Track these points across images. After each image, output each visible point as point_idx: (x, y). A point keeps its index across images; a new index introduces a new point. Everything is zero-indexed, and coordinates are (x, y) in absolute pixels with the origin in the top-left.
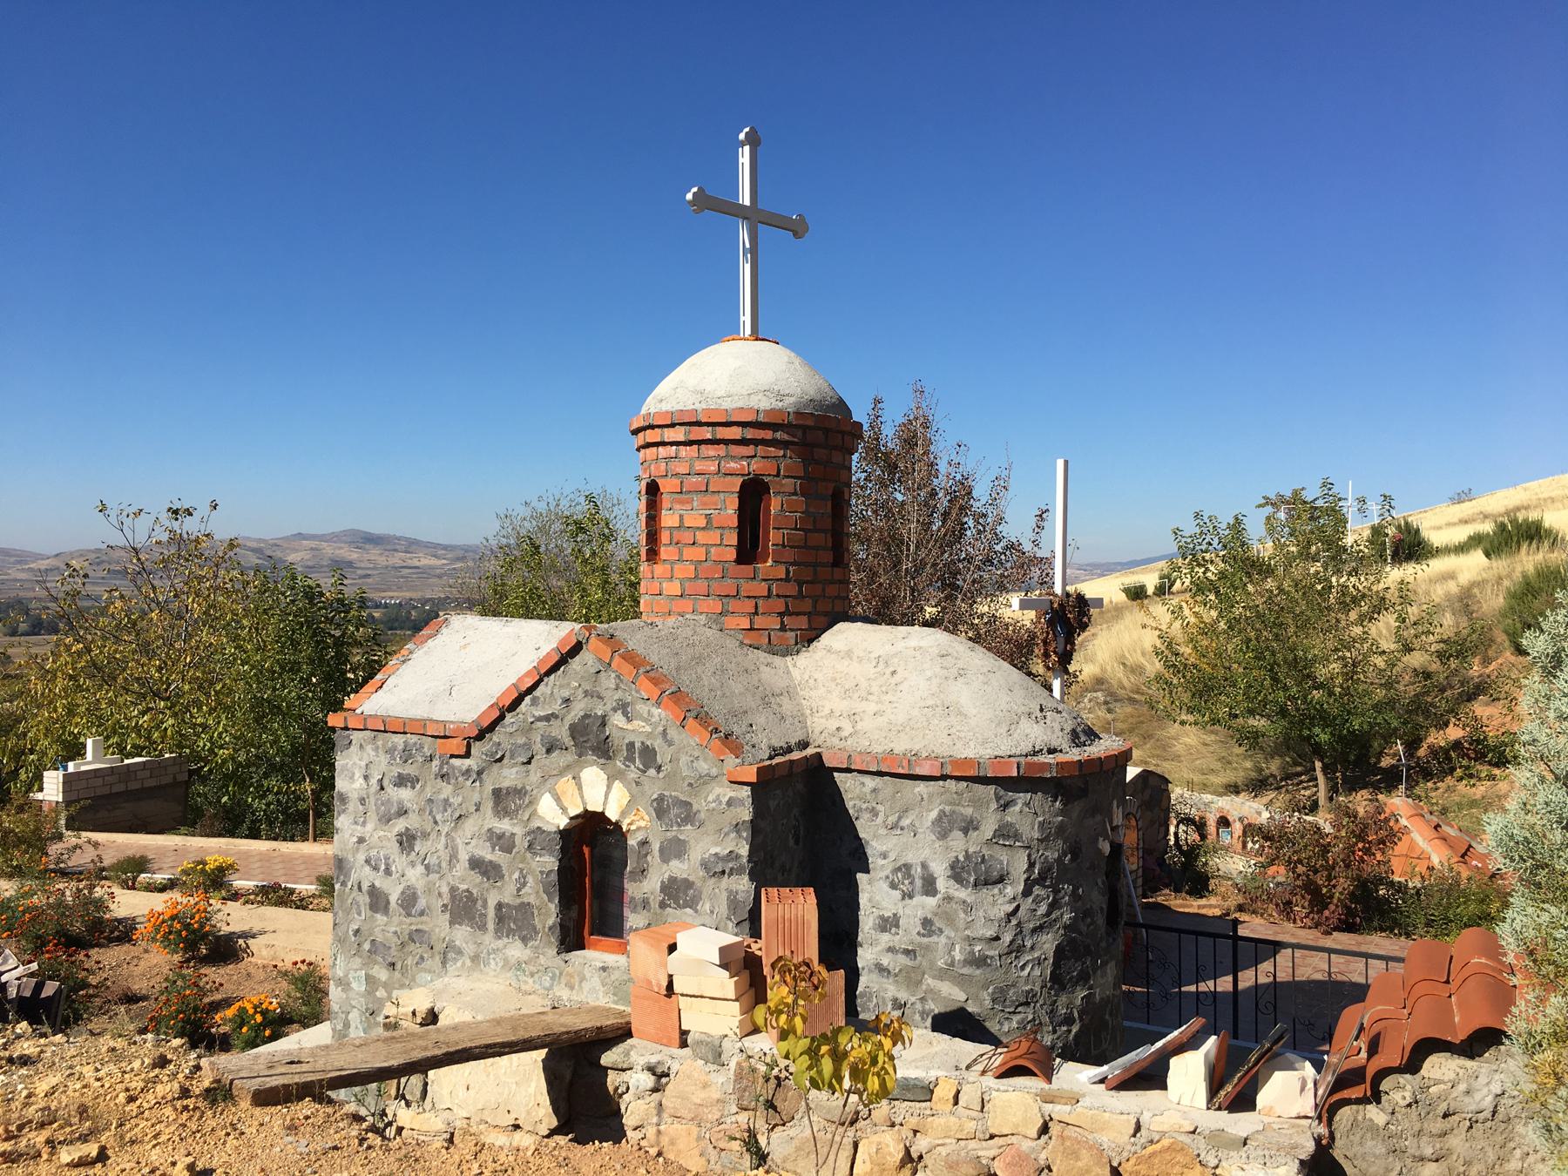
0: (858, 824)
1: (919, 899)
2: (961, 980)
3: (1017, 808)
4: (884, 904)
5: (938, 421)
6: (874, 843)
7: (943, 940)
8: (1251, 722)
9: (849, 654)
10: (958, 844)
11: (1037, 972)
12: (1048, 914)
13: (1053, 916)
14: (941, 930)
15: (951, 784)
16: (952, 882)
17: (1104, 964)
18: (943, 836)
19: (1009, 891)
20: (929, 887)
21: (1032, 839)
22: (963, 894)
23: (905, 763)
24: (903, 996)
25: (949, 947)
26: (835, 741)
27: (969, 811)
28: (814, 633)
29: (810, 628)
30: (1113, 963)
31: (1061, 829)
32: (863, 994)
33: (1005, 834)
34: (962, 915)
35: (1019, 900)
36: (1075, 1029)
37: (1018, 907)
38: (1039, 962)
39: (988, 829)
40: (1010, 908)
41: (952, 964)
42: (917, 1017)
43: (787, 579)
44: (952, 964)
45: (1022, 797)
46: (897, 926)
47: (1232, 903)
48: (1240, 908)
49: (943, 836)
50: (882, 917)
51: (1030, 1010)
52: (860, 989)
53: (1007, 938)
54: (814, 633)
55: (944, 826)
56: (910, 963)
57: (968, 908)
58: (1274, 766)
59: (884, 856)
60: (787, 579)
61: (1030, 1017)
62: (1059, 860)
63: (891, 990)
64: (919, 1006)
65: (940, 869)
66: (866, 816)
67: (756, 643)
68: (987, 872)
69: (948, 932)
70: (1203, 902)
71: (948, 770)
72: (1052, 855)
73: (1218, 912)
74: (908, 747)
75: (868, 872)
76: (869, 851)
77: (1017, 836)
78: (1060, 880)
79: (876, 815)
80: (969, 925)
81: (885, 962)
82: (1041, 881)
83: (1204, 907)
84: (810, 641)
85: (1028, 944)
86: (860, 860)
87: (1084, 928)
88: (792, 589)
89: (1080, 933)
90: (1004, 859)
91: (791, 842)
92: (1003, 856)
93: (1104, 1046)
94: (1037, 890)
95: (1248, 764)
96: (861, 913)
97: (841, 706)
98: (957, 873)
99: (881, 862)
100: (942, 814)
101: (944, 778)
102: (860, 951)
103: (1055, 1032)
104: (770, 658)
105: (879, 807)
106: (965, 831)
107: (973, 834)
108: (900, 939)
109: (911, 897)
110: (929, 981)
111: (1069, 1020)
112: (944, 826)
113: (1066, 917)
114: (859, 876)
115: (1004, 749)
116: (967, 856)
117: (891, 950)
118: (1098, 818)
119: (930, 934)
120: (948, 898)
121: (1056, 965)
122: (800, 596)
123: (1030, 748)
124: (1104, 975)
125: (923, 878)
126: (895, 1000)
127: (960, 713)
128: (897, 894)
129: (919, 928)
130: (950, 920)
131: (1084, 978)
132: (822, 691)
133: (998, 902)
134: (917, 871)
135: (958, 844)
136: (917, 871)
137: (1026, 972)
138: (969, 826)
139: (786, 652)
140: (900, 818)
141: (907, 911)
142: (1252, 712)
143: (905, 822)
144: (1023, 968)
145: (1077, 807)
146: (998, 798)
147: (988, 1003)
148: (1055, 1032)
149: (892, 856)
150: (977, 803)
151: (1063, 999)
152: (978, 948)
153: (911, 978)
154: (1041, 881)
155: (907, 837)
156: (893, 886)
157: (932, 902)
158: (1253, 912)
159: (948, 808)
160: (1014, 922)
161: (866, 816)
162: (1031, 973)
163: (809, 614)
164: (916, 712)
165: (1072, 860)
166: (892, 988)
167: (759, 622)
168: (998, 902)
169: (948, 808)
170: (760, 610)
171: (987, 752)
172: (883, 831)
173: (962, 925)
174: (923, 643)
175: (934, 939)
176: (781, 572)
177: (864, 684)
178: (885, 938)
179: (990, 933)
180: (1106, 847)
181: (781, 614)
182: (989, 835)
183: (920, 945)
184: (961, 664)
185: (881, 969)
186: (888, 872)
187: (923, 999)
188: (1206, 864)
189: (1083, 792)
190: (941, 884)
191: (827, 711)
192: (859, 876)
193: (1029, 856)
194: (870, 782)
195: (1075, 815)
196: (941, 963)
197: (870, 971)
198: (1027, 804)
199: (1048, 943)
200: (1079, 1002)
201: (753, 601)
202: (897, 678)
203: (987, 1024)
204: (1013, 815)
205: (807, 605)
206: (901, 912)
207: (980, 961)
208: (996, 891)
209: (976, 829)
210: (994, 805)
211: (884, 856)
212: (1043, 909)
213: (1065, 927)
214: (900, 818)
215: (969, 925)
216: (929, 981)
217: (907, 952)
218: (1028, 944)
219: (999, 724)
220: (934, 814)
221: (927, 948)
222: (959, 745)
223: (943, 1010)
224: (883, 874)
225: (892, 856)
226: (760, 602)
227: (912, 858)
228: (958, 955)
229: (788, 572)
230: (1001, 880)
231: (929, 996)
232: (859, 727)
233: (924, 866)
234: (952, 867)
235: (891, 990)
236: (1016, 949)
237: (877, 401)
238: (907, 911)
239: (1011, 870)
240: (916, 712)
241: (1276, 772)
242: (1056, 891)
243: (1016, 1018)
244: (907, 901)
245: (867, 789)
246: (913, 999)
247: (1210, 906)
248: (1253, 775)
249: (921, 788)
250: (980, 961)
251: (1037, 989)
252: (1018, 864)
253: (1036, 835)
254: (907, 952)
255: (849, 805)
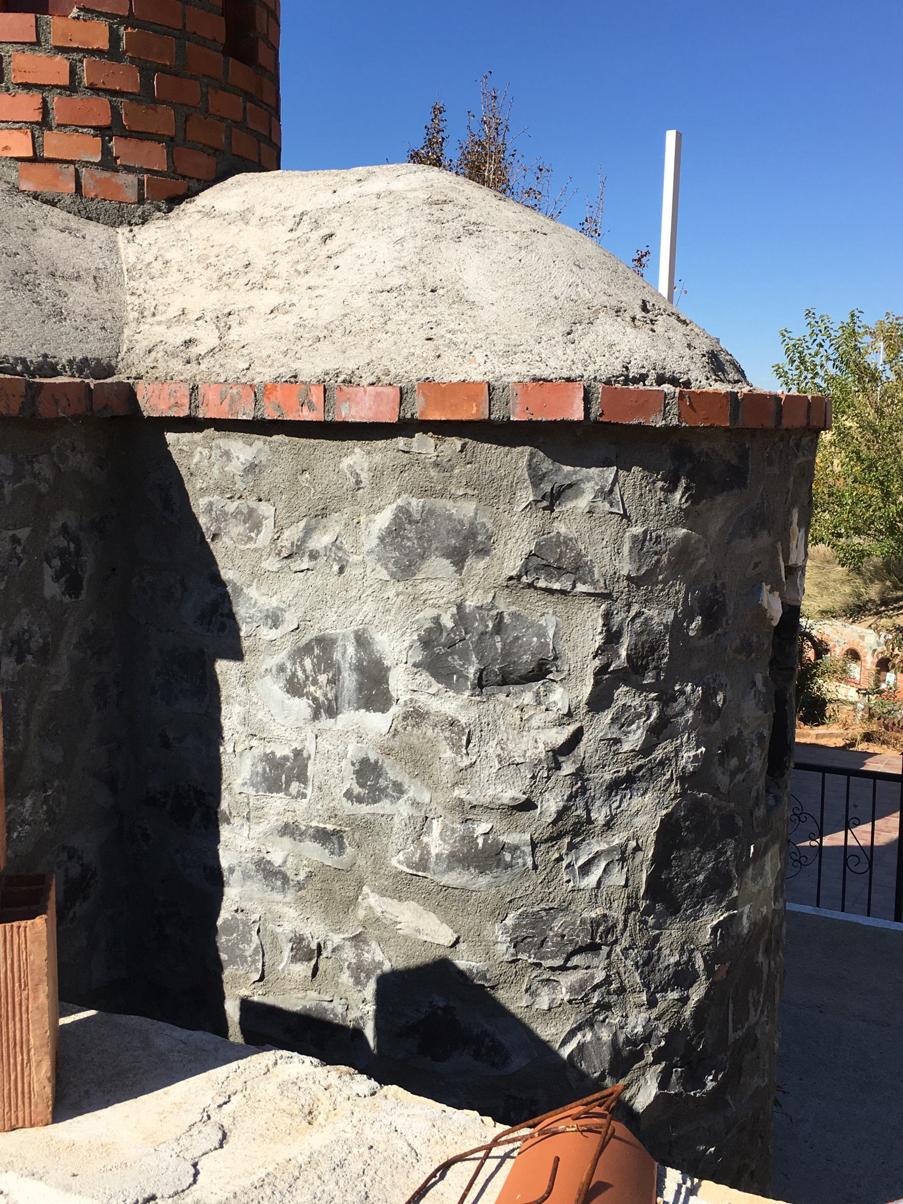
0: (218, 549)
1: (352, 717)
2: (442, 900)
3: (582, 503)
4: (276, 730)
5: (512, 141)
6: (252, 592)
7: (403, 808)
8: (856, 540)
9: (244, 216)
10: (441, 589)
11: (617, 878)
12: (646, 749)
13: (658, 754)
14: (399, 789)
15: (424, 445)
16: (424, 677)
17: (760, 854)
18: (406, 569)
19: (559, 698)
20: (374, 690)
21: (615, 577)
22: (451, 704)
23: (316, 396)
24: (315, 930)
25: (418, 824)
26: (176, 365)
27: (466, 510)
28: (181, 186)
29: (173, 172)
30: (776, 848)
31: (683, 555)
32: (231, 927)
33: (551, 565)
34: (448, 754)
35: (582, 718)
36: (696, 994)
37: (577, 736)
38: (623, 855)
39: (511, 556)
40: (560, 736)
41: (423, 864)
42: (346, 978)
43: (113, 53)
44: (423, 864)
45: (594, 478)
46: (302, 777)
47: (858, 730)
48: (868, 737)
49: (406, 569)
50: (269, 759)
51: (599, 961)
52: (225, 914)
53: (551, 804)
54: (181, 186)
55: (408, 547)
56: (331, 861)
57: (463, 736)
58: (873, 592)
59: (274, 619)
60: (113, 53)
61: (600, 976)
62: (676, 629)
63: (291, 918)
64: (349, 954)
65: (396, 647)
66: (236, 529)
67: (47, 191)
68: (506, 654)
69: (415, 790)
70: (821, 730)
71: (420, 408)
72: (660, 616)
73: (840, 743)
74: (331, 366)
75: (237, 654)
76: (241, 611)
77: (579, 569)
78: (676, 672)
79: (257, 526)
80: (463, 775)
81: (276, 858)
82: (632, 674)
83: (824, 736)
84: (174, 200)
85: (599, 816)
86: (217, 627)
87: (723, 780)
88: (125, 78)
89: (715, 790)
90: (549, 623)
91: (52, 589)
92: (546, 617)
93: (753, 1018)
94: (623, 696)
95: (847, 589)
96: (226, 749)
97: (200, 298)
98: (437, 655)
99: (268, 634)
100: (403, 518)
101: (406, 427)
102: (225, 832)
103: (652, 1003)
104: (75, 222)
105: (266, 509)
106: (458, 557)
107: (476, 565)
108: (306, 809)
109: (332, 712)
110: (373, 901)
111: (683, 977)
112: (408, 547)
113: (687, 755)
114: (223, 667)
115: (557, 362)
116: (462, 616)
117: (288, 830)
118: (764, 539)
119: (375, 795)
120: (416, 715)
121: (661, 860)
122: (144, 96)
123: (618, 369)
124: (760, 873)
125: (359, 669)
126: (298, 941)
127: (460, 299)
128: (301, 706)
129: (350, 783)
130: (420, 764)
131: (718, 886)
132: (174, 278)
133: (531, 725)
134: (347, 654)
135: (441, 589)
136: (347, 654)
137: (591, 880)
138: (466, 547)
139: (119, 217)
140: (308, 532)
141: (325, 745)
142: (858, 531)
143: (321, 541)
144: (585, 869)
145: (720, 511)
146: (537, 478)
147: (503, 949)
148: (652, 1003)
149: (291, 620)
150: (487, 490)
151: (673, 933)
152: (482, 828)
153: (333, 892)
154: (632, 674)
155: (325, 577)
156: (294, 688)
157: (377, 723)
158: (883, 743)
159: (416, 504)
160: (568, 768)
161: (236, 529)
162: (601, 881)
163: (170, 142)
164: (361, 301)
165: (705, 629)
166: (291, 913)
167: (55, 144)
168: (531, 725)
169: (416, 504)
170: (56, 118)
171: (514, 371)
172: (271, 564)
173: (445, 773)
174: (398, 185)
175: (384, 806)
176: (97, 35)
177: (261, 261)
178: (277, 803)
179: (511, 793)
180: (775, 608)
181: (101, 131)
182: (513, 566)
183: (352, 820)
184: (472, 216)
185: (269, 873)
186: (281, 657)
187: (358, 940)
188: (819, 689)
189: (735, 477)
190: (399, 682)
191: (173, 311)
192: (223, 667)
193: (607, 616)
194: (242, 450)
195: (716, 524)
196: (397, 862)
197: (246, 876)
198: (607, 494)
199: (645, 813)
200: (706, 937)
201: (36, 99)
202: (333, 245)
203: (502, 995)
204: (572, 520)
205: (163, 120)
206: (310, 747)
207: (487, 858)
208: (528, 698)
209: (483, 552)
210: (527, 495)
211: (274, 619)
212: (635, 738)
213: (683, 779)
214: (308, 532)
215: (463, 775)
216: (373, 901)
217: (323, 836)
218: (599, 816)
219: (548, 319)
220: (384, 519)
221: (367, 826)
222: (449, 356)
223: (401, 964)
224: (272, 662)
225: (291, 620)
226: (55, 101)
227: (336, 623)
228: (436, 843)
229: (114, 38)
230: (540, 671)
231: (372, 932)
232: (233, 335)
233: (362, 641)
234: (426, 642)
235: (291, 918)
236: (570, 829)
237: (438, 111)
238: (324, 745)
239: (564, 648)
240: (361, 301)
241: (876, 598)
242: (666, 698)
243: (567, 980)
244: (325, 722)
245: (235, 467)
246: (337, 939)
247: (831, 735)
248: (851, 600)
249: (357, 457)
250: (487, 858)
251: (617, 914)
252: (579, 635)
253: (626, 568)
254: (323, 836)
255: (199, 505)
